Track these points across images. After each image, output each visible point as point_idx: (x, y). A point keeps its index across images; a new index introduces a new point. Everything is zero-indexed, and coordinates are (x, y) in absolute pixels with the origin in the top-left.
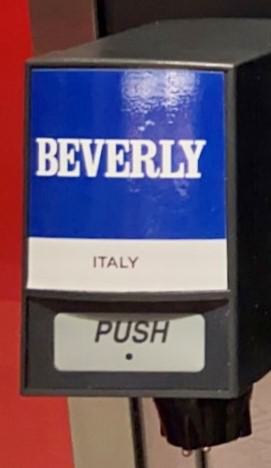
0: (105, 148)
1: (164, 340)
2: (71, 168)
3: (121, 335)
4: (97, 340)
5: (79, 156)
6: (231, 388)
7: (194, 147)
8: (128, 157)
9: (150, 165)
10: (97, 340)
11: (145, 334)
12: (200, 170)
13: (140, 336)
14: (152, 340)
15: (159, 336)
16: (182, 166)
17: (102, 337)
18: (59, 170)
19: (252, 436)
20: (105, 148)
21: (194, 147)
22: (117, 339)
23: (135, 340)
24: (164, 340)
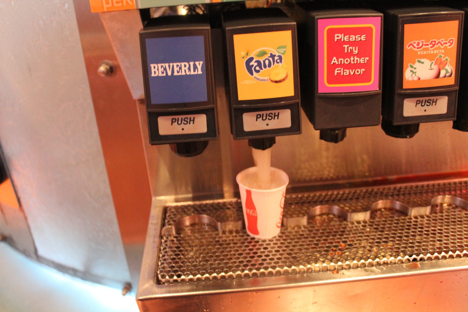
0: (173, 66)
5: (165, 69)
7: (200, 64)
8: (180, 68)
13: (270, 118)
20: (173, 66)
22: (263, 119)
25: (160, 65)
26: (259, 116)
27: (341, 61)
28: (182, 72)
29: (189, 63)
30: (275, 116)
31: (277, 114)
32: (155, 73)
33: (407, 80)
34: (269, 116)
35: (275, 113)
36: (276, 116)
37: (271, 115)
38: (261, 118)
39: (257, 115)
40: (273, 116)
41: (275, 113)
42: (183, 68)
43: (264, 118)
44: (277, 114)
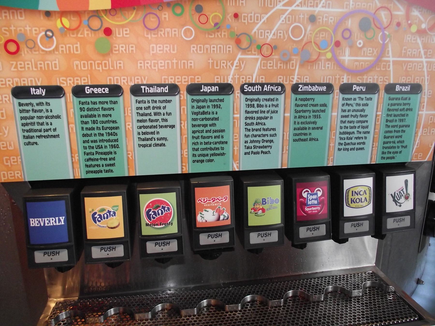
9: (54, 223)
11: (217, 236)
17: (45, 255)
21: (62, 218)
22: (159, 246)
30: (317, 228)
31: (168, 242)
35: (56, 252)
40: (218, 235)
41: (56, 252)
42: (51, 221)
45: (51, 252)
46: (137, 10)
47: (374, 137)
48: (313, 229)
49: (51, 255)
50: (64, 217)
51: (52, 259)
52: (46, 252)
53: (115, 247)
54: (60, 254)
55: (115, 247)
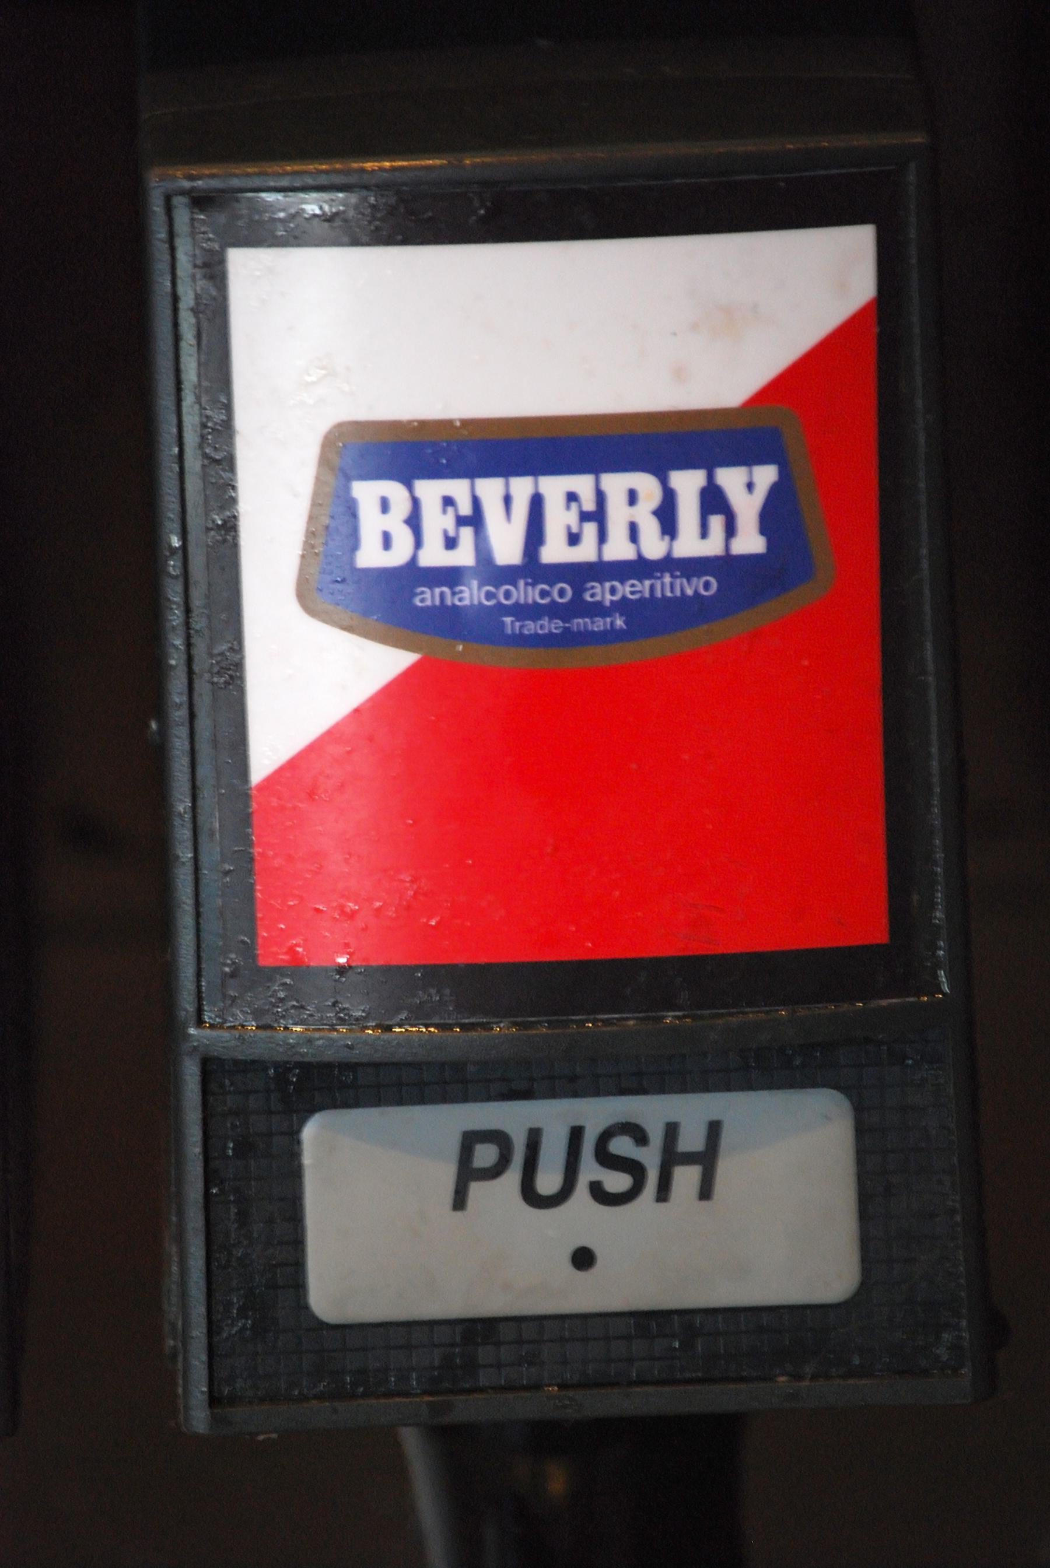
0: (537, 503)
1: (706, 1192)
2: (451, 543)
3: (548, 1182)
4: (460, 1201)
5: (475, 520)
6: (575, 624)
7: (750, 486)
8: (598, 516)
9: (650, 528)
10: (460, 1201)
11: (635, 1169)
12: (763, 530)
13: (617, 1182)
14: (663, 1192)
15: (686, 1177)
16: (717, 523)
17: (477, 1189)
18: (418, 543)
19: (465, 1213)
20: (537, 503)
21: (750, 486)
22: (531, 1196)
23: (598, 1193)
24: (706, 1192)
25: (430, 491)
26: (485, 1155)
27: (442, 595)
28: (602, 537)
29: (410, 487)
30: (671, 1158)
31: (691, 1140)
32: (387, 541)
33: (329, 214)
34: (606, 1159)
35: (672, 1130)
36: (689, 1159)
37: (622, 1146)
38: (512, 1177)
39: (470, 1140)
40: (650, 1158)
41: (672, 1130)
42: (618, 515)
43: (548, 1182)
44: (691, 1140)
45: (576, 1134)
46: (179, 957)
47: (207, 1194)
48: (590, 1171)
49: (581, 1191)
50: (766, 475)
51: (583, 1259)
52: (500, 1138)
53: (714, 1129)
54: (724, 1167)
55: (714, 1129)
